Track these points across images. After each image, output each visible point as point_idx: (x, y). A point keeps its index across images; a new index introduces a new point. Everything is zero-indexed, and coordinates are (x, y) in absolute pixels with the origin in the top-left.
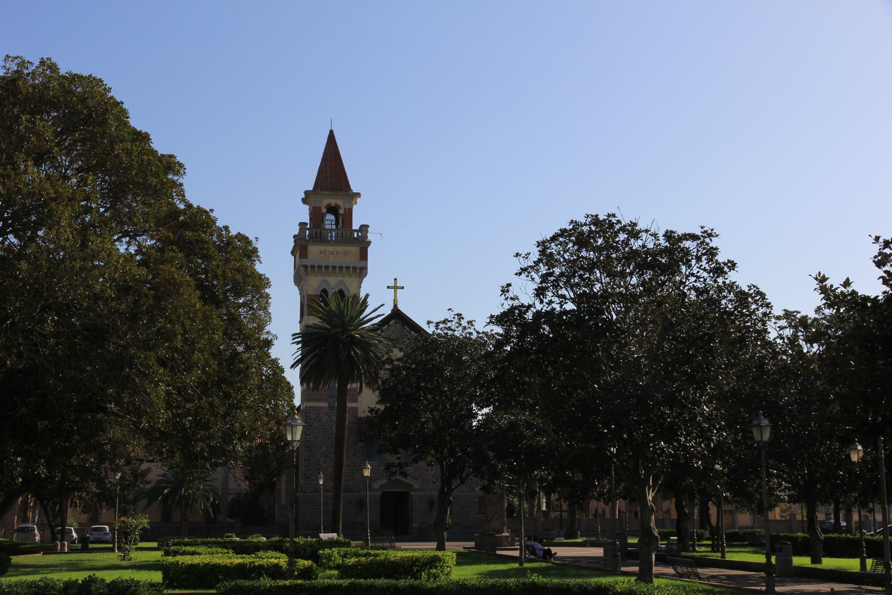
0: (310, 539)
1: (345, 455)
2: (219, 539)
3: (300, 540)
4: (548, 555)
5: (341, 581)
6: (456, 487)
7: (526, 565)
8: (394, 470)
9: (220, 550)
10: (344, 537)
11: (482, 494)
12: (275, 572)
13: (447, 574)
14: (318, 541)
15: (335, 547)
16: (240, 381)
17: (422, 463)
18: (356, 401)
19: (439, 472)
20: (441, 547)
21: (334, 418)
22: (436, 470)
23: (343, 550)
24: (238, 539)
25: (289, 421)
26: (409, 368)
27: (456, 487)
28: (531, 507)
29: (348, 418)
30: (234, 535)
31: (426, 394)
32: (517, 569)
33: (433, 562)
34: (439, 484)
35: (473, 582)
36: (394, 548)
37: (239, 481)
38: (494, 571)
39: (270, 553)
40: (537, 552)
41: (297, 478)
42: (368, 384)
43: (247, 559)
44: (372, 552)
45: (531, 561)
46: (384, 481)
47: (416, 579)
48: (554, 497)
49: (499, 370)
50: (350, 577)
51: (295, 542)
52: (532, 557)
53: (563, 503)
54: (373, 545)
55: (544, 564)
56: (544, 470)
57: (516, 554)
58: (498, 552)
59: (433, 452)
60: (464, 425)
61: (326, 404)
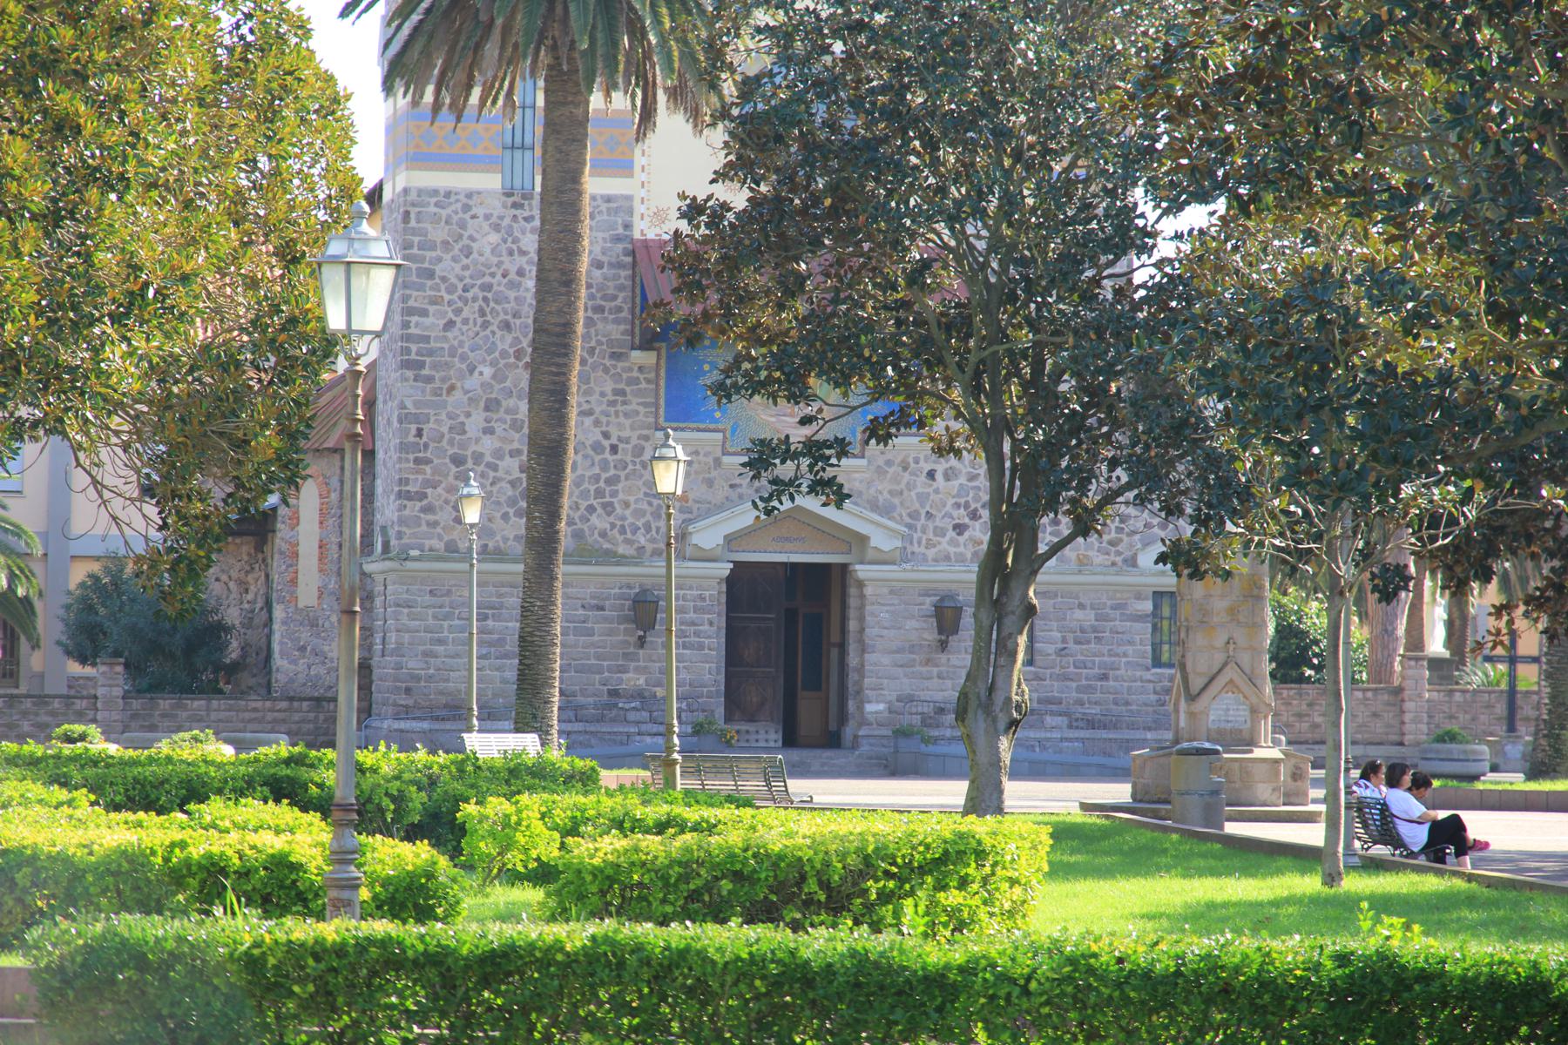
0: (421, 756)
1: (574, 399)
2: (32, 748)
3: (383, 760)
4: (1448, 839)
5: (558, 931)
6: (1055, 549)
7: (1354, 883)
8: (786, 470)
9: (36, 790)
10: (570, 749)
11: (1167, 578)
12: (278, 888)
13: (1011, 914)
14: (460, 766)
15: (531, 789)
16: (119, 67)
17: (907, 443)
18: (624, 167)
19: (983, 482)
20: (985, 800)
21: (530, 242)
22: (969, 477)
23: (568, 802)
24: (113, 749)
25: (335, 248)
26: (860, 26)
27: (1055, 549)
28: (1383, 637)
29: (592, 243)
30: (93, 730)
31: (931, 145)
32: (1315, 901)
33: (945, 863)
34: (980, 533)
35: (1123, 946)
36: (784, 800)
37: (117, 504)
38: (1211, 906)
39: (253, 809)
40: (1404, 830)
41: (369, 496)
42: (677, 95)
43: (152, 833)
44: (692, 815)
45: (1374, 866)
46: (745, 517)
47: (876, 928)
48: (1483, 598)
49: (1262, 37)
50: (600, 914)
51: (361, 769)
52: (1380, 850)
53: (1521, 624)
54: (693, 784)
55: (1430, 883)
56: (1442, 481)
57: (1312, 835)
58: (1231, 828)
59: (956, 394)
60: (1096, 282)
61: (491, 182)
